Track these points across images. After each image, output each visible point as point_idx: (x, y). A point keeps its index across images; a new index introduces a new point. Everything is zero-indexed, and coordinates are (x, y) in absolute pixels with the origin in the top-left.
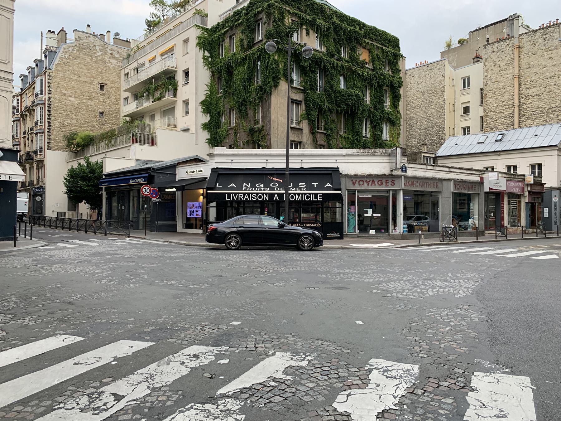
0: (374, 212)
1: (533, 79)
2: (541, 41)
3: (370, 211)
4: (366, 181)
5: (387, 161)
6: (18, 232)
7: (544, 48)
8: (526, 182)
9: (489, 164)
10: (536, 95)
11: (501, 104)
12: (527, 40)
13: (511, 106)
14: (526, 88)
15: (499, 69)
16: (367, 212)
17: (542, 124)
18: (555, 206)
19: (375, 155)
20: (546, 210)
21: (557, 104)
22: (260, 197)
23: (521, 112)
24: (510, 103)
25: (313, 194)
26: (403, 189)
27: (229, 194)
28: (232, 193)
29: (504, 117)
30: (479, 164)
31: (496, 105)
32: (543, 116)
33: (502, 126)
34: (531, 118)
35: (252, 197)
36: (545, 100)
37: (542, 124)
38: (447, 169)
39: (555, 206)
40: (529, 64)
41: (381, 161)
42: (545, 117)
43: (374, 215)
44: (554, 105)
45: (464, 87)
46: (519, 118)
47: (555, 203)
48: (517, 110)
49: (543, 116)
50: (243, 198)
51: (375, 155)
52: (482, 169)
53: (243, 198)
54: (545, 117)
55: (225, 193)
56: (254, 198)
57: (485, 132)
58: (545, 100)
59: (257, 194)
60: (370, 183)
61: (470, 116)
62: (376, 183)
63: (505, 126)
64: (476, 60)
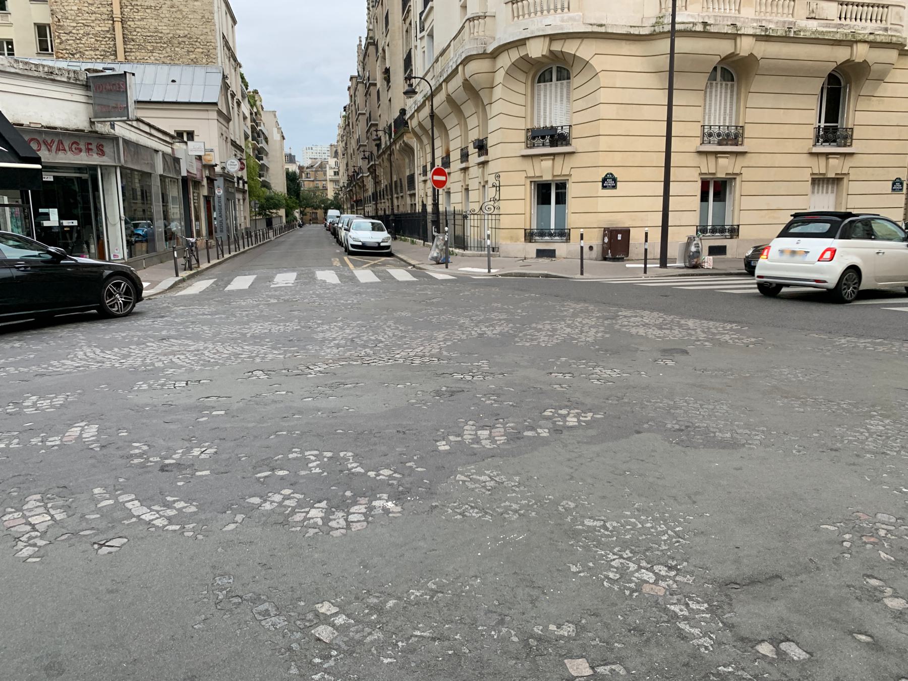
0: (61, 217)
3: (54, 213)
4: (45, 143)
5: (83, 99)
8: (204, 162)
9: (184, 125)
10: (150, 7)
11: (86, 9)
13: (105, 17)
16: (47, 216)
17: (164, 63)
18: (219, 202)
19: (54, 80)
21: (186, 32)
23: (126, 32)
26: (122, 168)
29: (95, 35)
30: (170, 123)
31: (75, 8)
32: (165, 48)
33: (92, 52)
34: (145, 48)
36: (165, 20)
37: (164, 63)
38: (147, 129)
39: (219, 202)
41: (68, 97)
42: (168, 50)
43: (66, 223)
44: (181, 33)
46: (125, 43)
47: (219, 197)
48: (118, 26)
49: (165, 48)
51: (54, 80)
52: (172, 133)
54: (168, 50)
57: (58, 58)
60: (54, 147)
61: (10, 19)
62: (67, 148)
63: (98, 53)
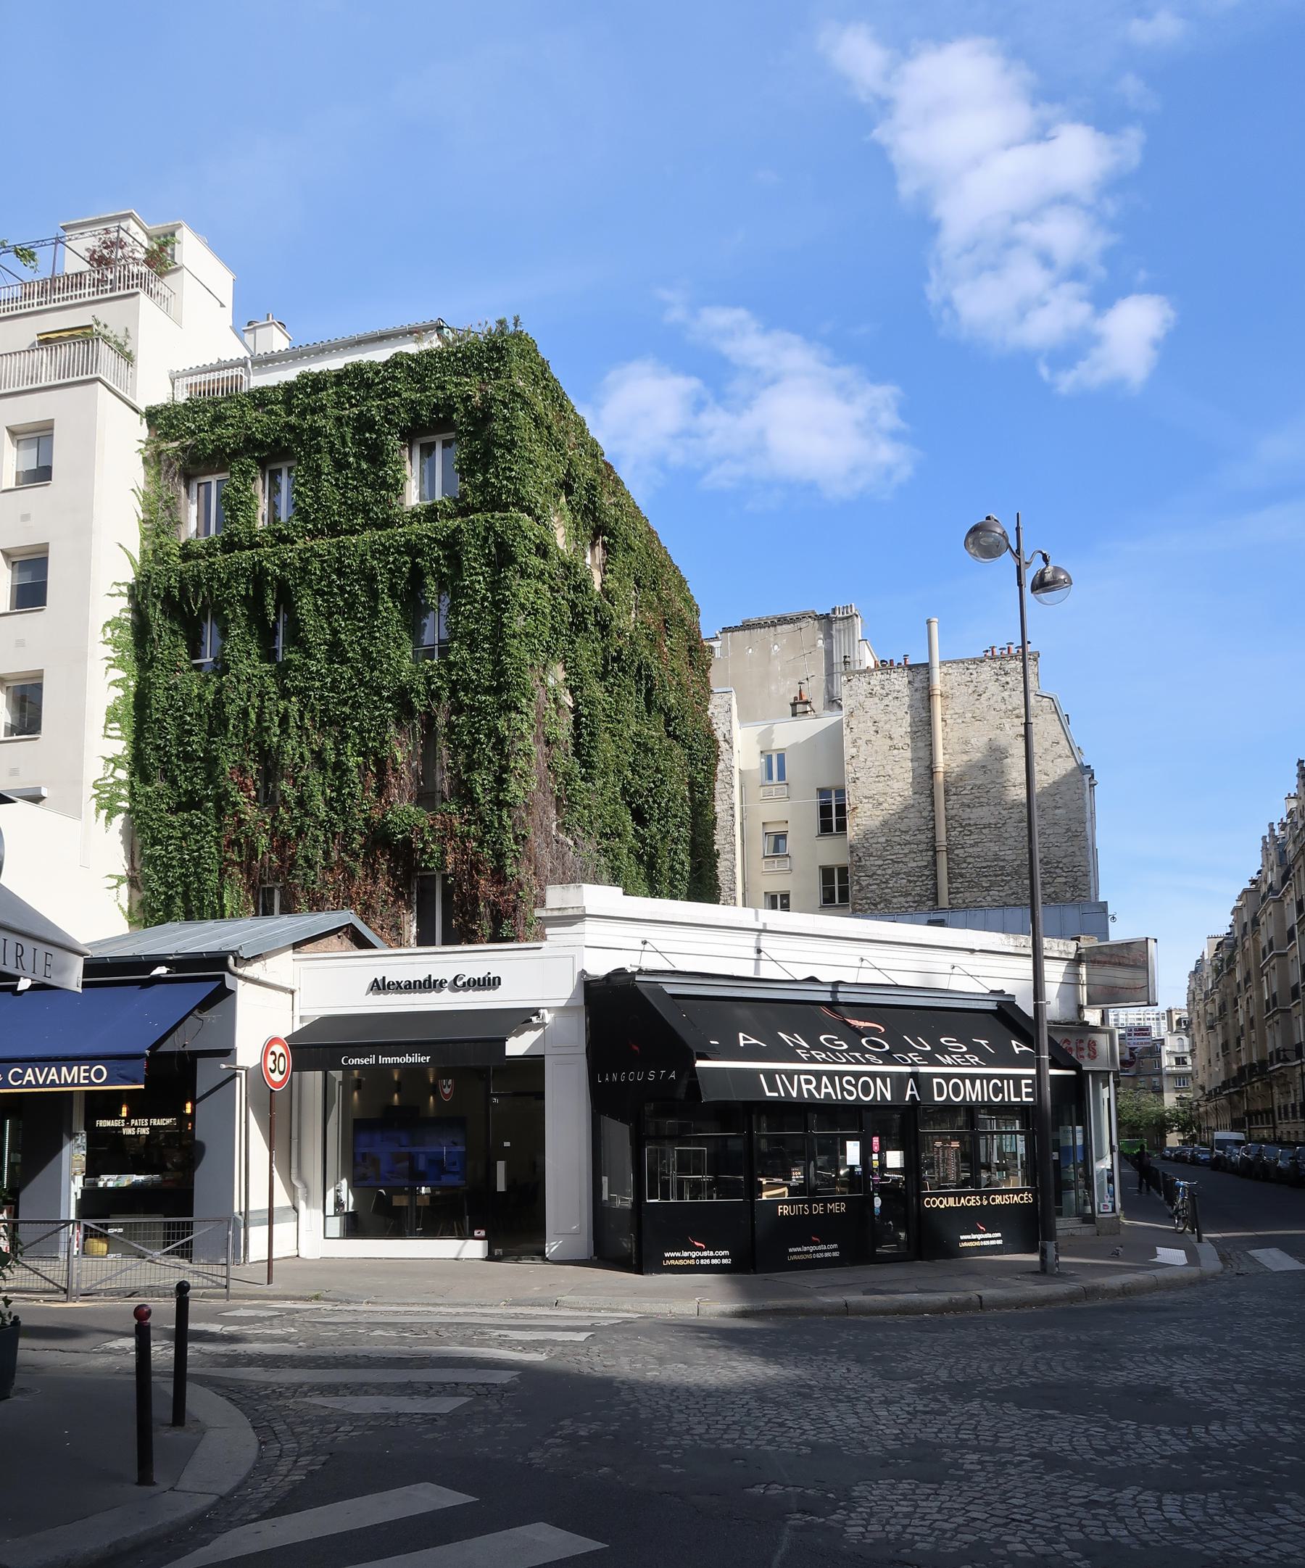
1: (978, 782)
2: (994, 688)
6: (240, 1348)
7: (1004, 707)
10: (988, 826)
11: (897, 839)
12: (959, 679)
13: (923, 847)
14: (963, 804)
15: (889, 742)
20: (189, 1105)
22: (956, 1090)
24: (922, 837)
25: (1008, 1077)
27: (770, 1074)
28: (780, 1072)
31: (883, 839)
33: (902, 899)
34: (978, 885)
35: (843, 1089)
36: (1010, 842)
40: (967, 743)
42: (1013, 884)
45: (770, 777)
49: (1008, 882)
50: (818, 1088)
53: (818, 1088)
54: (1013, 884)
55: (756, 1072)
56: (850, 1093)
58: (1010, 842)
59: (857, 1075)
63: (910, 899)
64: (800, 708)
